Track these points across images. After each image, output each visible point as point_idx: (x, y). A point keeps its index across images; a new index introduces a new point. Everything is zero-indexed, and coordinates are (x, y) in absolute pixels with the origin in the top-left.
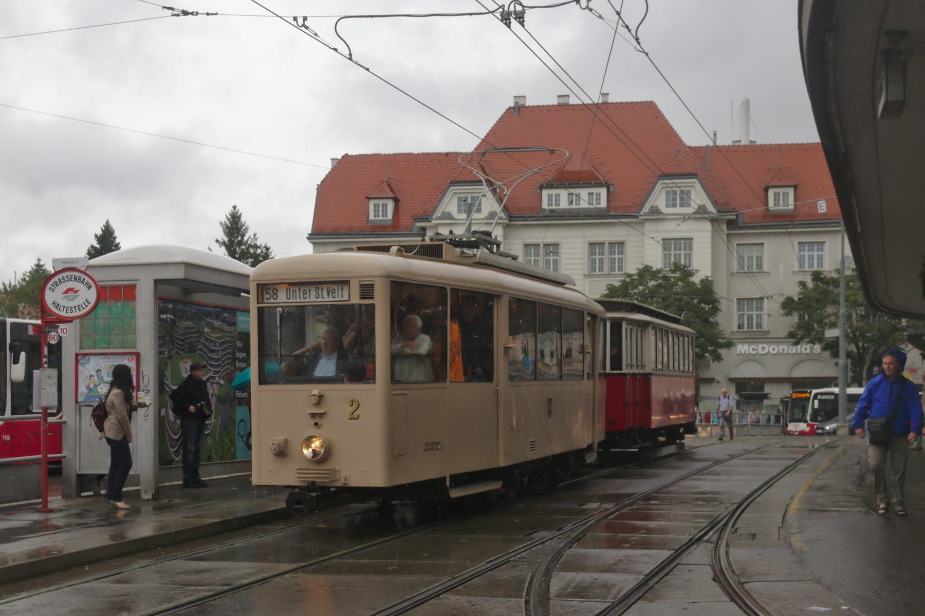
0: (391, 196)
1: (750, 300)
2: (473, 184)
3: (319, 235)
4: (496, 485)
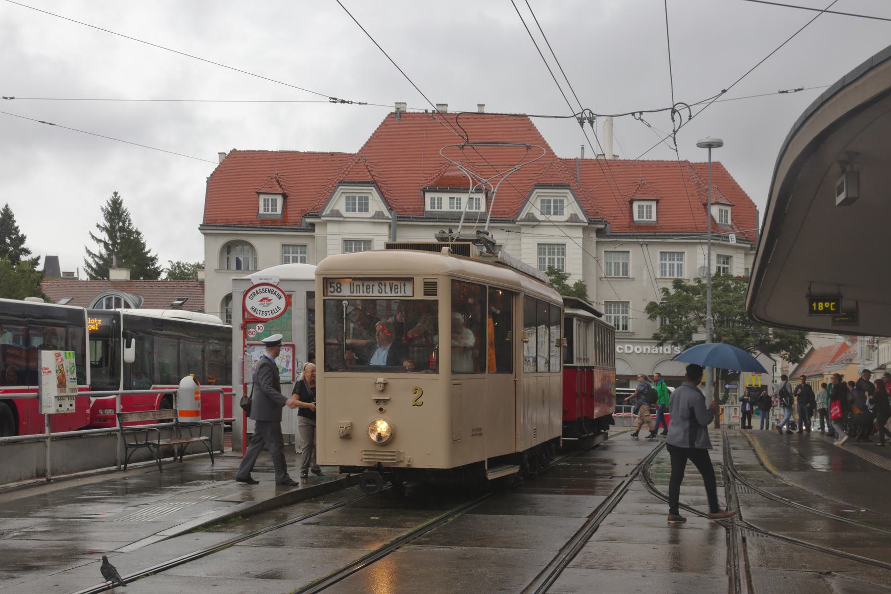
1: (616, 303)
2: (361, 185)
3: (210, 226)
4: (515, 470)
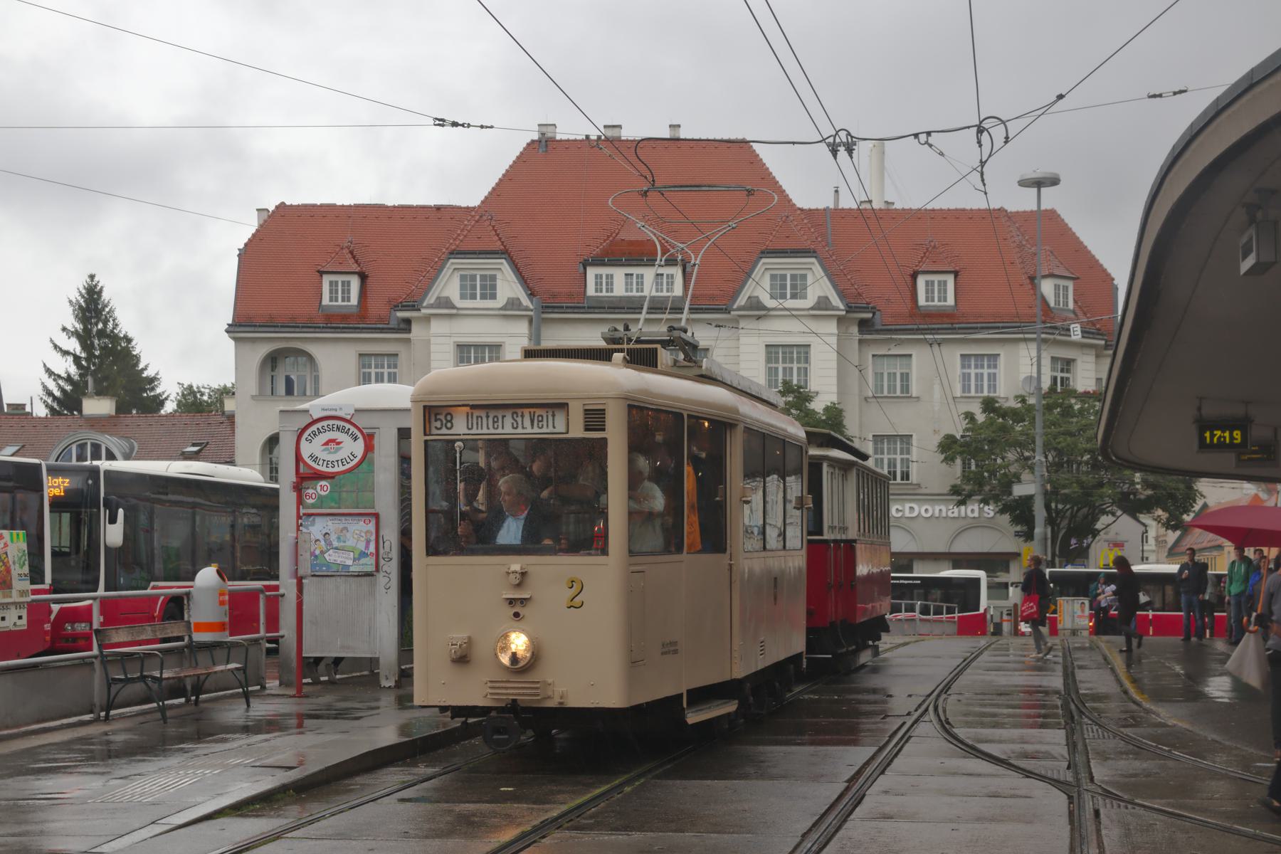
0: (357, 270)
1: (891, 438)
